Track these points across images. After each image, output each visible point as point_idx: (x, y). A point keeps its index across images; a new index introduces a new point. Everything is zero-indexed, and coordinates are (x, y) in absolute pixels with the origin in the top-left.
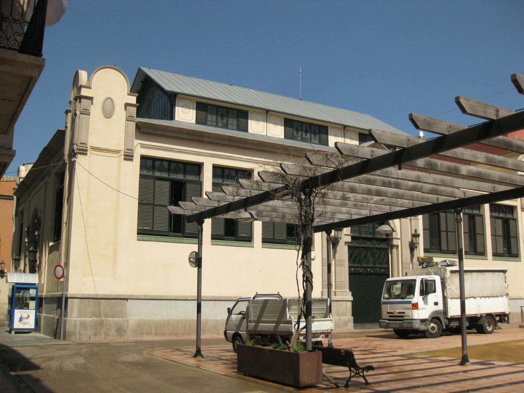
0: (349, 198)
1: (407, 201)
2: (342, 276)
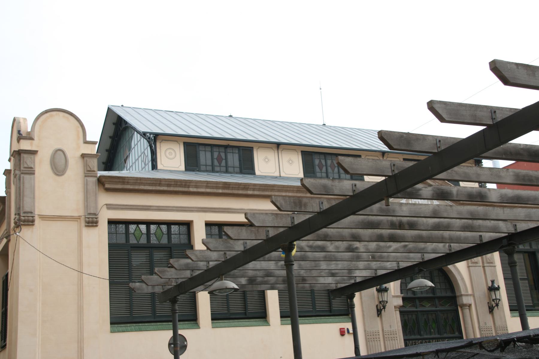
0: (357, 248)
1: (441, 245)
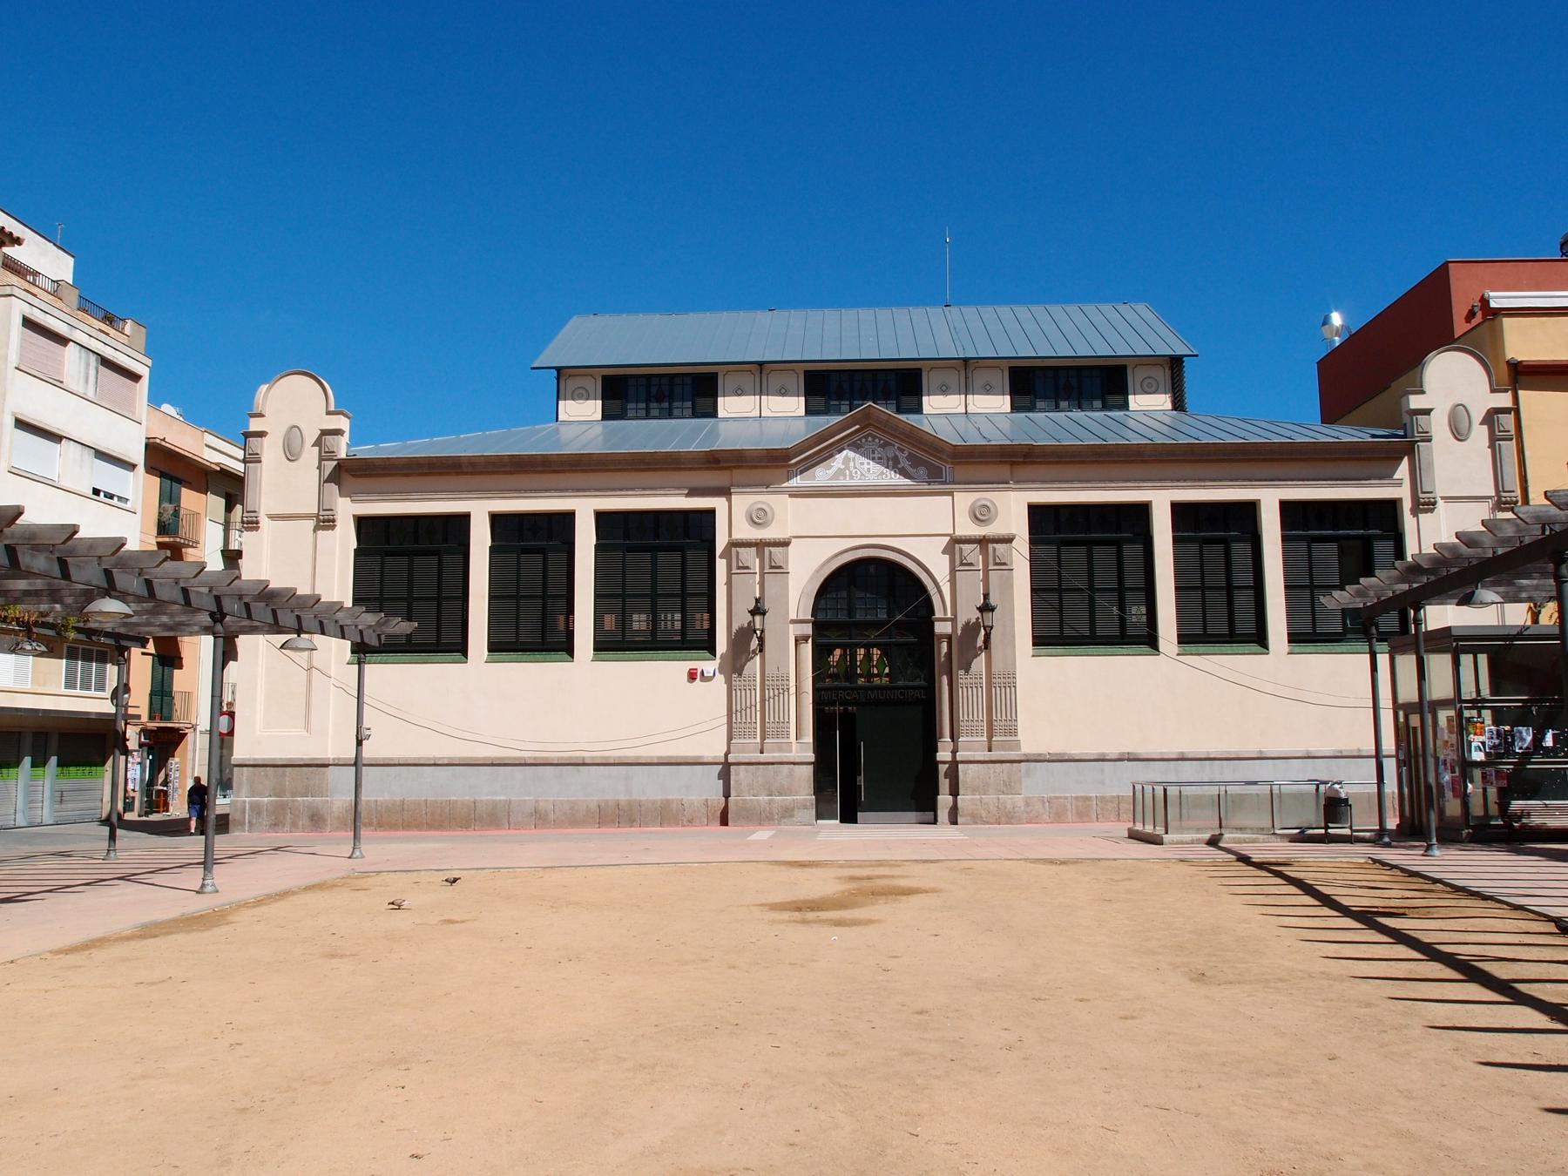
2: (753, 708)
